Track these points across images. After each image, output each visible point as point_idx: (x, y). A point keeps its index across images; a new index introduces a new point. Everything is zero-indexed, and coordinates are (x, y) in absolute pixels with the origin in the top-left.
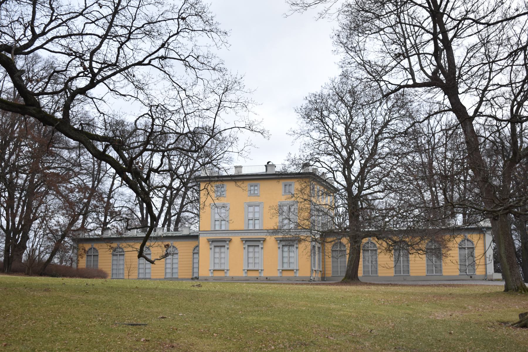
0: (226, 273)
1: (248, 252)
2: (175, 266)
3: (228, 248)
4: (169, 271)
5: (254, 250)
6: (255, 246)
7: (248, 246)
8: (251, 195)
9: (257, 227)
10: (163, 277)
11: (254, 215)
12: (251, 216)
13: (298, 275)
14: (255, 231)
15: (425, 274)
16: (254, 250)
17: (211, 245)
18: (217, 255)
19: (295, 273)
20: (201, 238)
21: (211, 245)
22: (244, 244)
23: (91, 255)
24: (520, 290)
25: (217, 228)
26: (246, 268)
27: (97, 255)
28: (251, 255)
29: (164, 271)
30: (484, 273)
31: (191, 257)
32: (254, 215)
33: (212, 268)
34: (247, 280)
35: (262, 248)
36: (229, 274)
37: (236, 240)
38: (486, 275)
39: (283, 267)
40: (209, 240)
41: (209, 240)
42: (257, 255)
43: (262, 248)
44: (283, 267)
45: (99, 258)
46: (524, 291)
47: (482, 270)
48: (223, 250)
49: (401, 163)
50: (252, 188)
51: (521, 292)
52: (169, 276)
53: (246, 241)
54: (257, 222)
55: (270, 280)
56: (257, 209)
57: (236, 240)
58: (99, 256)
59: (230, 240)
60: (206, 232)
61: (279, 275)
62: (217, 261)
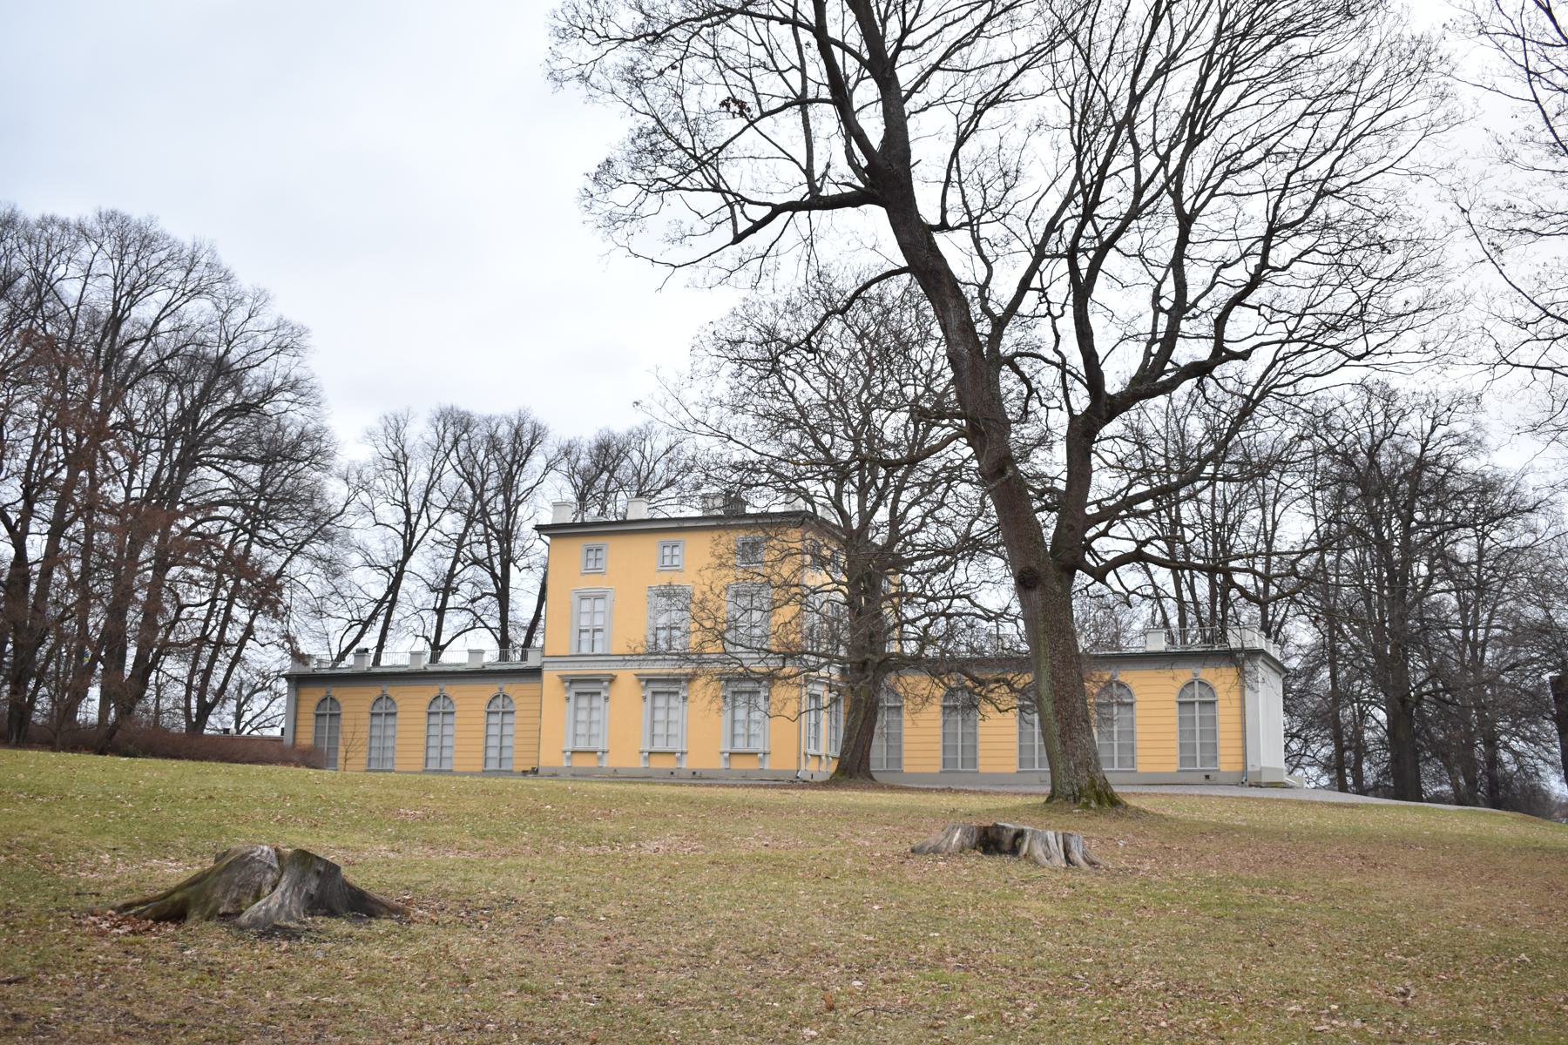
0: (600, 758)
1: (654, 709)
2: (447, 742)
3: (606, 699)
4: (493, 753)
5: (668, 702)
6: (592, 694)
7: (578, 694)
8: (663, 568)
9: (598, 650)
10: (479, 768)
11: (592, 619)
12: (585, 622)
13: (767, 767)
14: (594, 657)
15: (1175, 768)
16: (668, 702)
17: (567, 689)
18: (741, 714)
19: (761, 760)
20: (545, 674)
21: (567, 689)
22: (644, 688)
23: (1193, 703)
24: (1084, 800)
25: (585, 649)
26: (648, 748)
27: (1131, 704)
28: (582, 716)
29: (482, 755)
30: (1239, 768)
31: (483, 721)
32: (592, 619)
33: (570, 748)
34: (647, 777)
35: (685, 699)
36: (608, 762)
37: (626, 677)
38: (1244, 772)
39: (733, 745)
40: (563, 679)
41: (563, 679)
42: (595, 716)
43: (606, 699)
44: (733, 745)
45: (1138, 713)
46: (1100, 802)
47: (1233, 759)
48: (597, 702)
49: (1199, 501)
50: (667, 551)
51: (1087, 806)
52: (493, 765)
53: (648, 681)
54: (598, 635)
55: (700, 778)
56: (599, 605)
57: (626, 677)
58: (1137, 706)
59: (612, 680)
60: (558, 659)
61: (722, 765)
62: (581, 729)
